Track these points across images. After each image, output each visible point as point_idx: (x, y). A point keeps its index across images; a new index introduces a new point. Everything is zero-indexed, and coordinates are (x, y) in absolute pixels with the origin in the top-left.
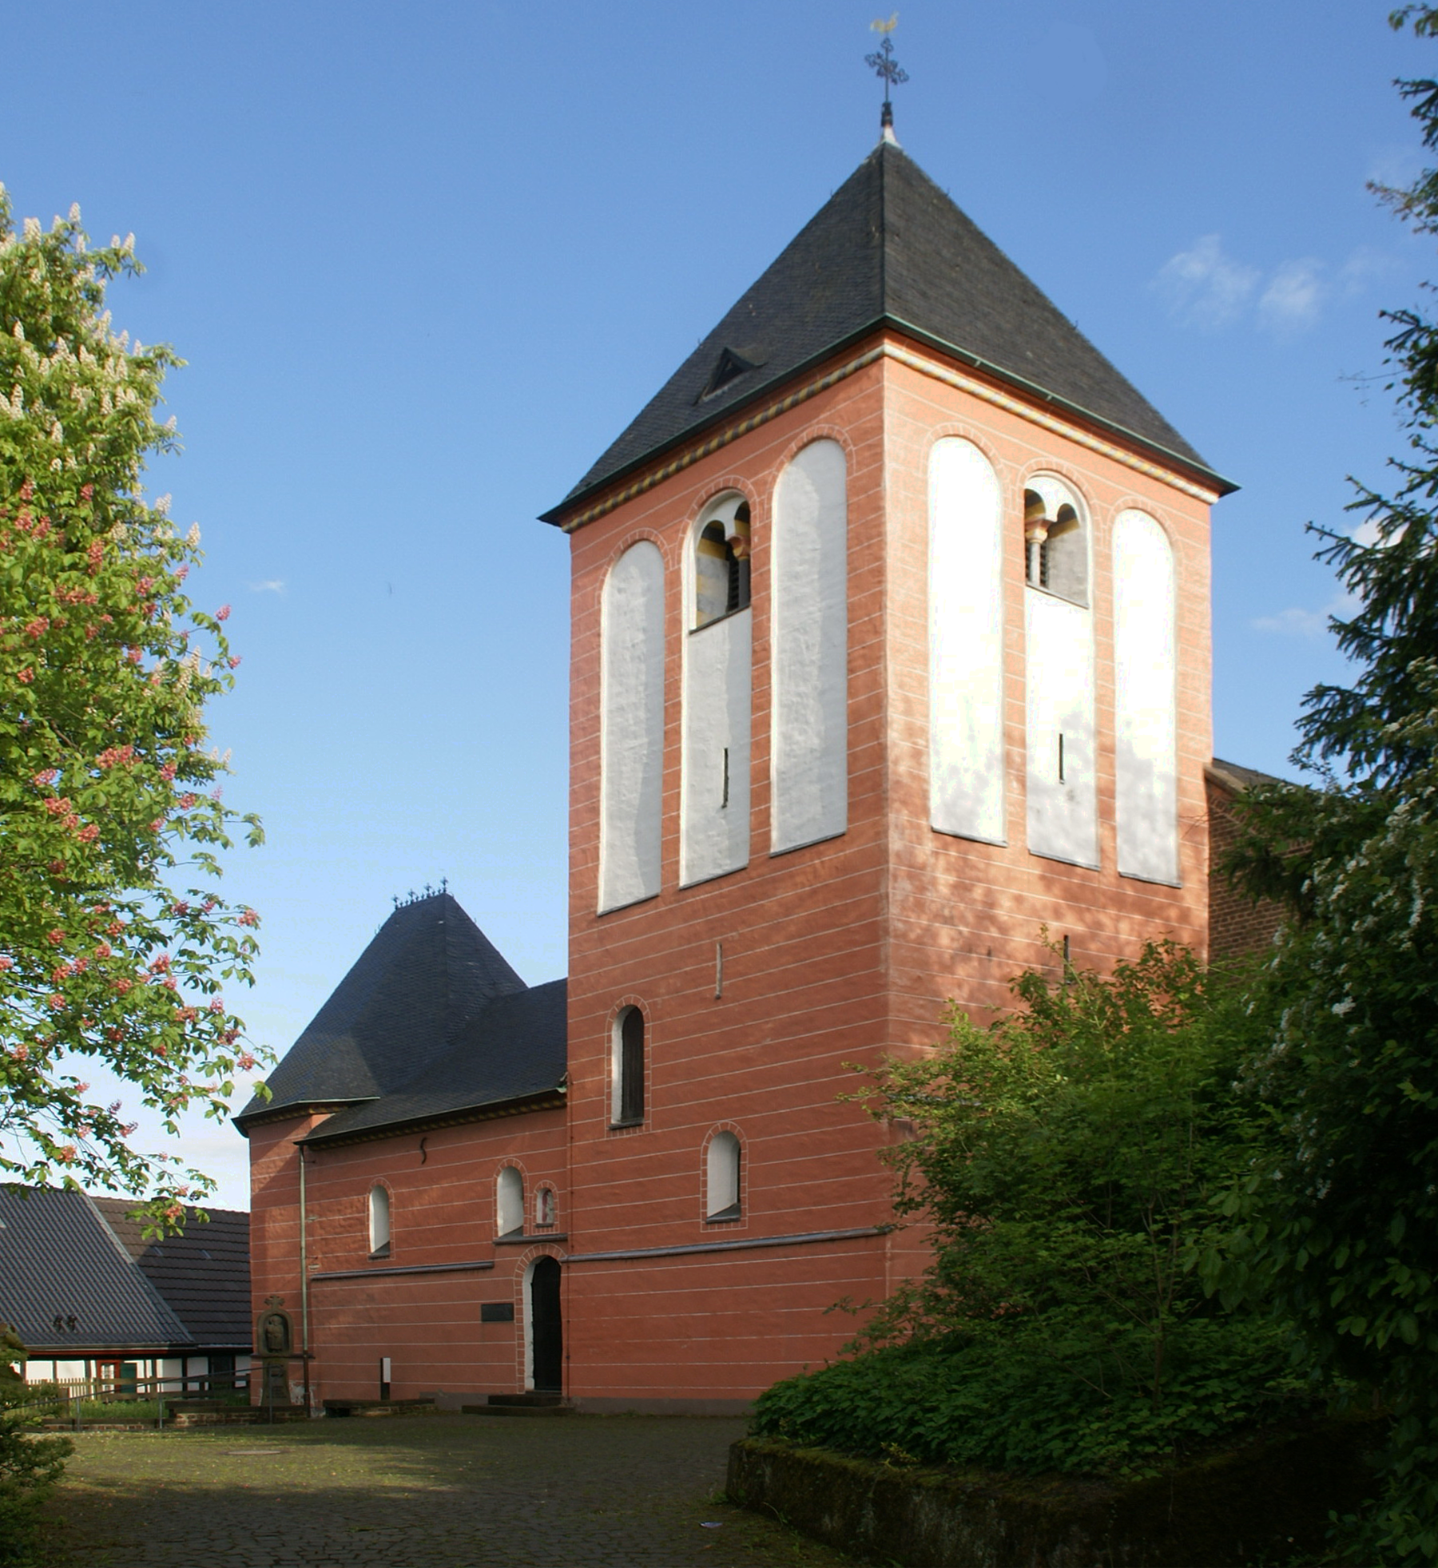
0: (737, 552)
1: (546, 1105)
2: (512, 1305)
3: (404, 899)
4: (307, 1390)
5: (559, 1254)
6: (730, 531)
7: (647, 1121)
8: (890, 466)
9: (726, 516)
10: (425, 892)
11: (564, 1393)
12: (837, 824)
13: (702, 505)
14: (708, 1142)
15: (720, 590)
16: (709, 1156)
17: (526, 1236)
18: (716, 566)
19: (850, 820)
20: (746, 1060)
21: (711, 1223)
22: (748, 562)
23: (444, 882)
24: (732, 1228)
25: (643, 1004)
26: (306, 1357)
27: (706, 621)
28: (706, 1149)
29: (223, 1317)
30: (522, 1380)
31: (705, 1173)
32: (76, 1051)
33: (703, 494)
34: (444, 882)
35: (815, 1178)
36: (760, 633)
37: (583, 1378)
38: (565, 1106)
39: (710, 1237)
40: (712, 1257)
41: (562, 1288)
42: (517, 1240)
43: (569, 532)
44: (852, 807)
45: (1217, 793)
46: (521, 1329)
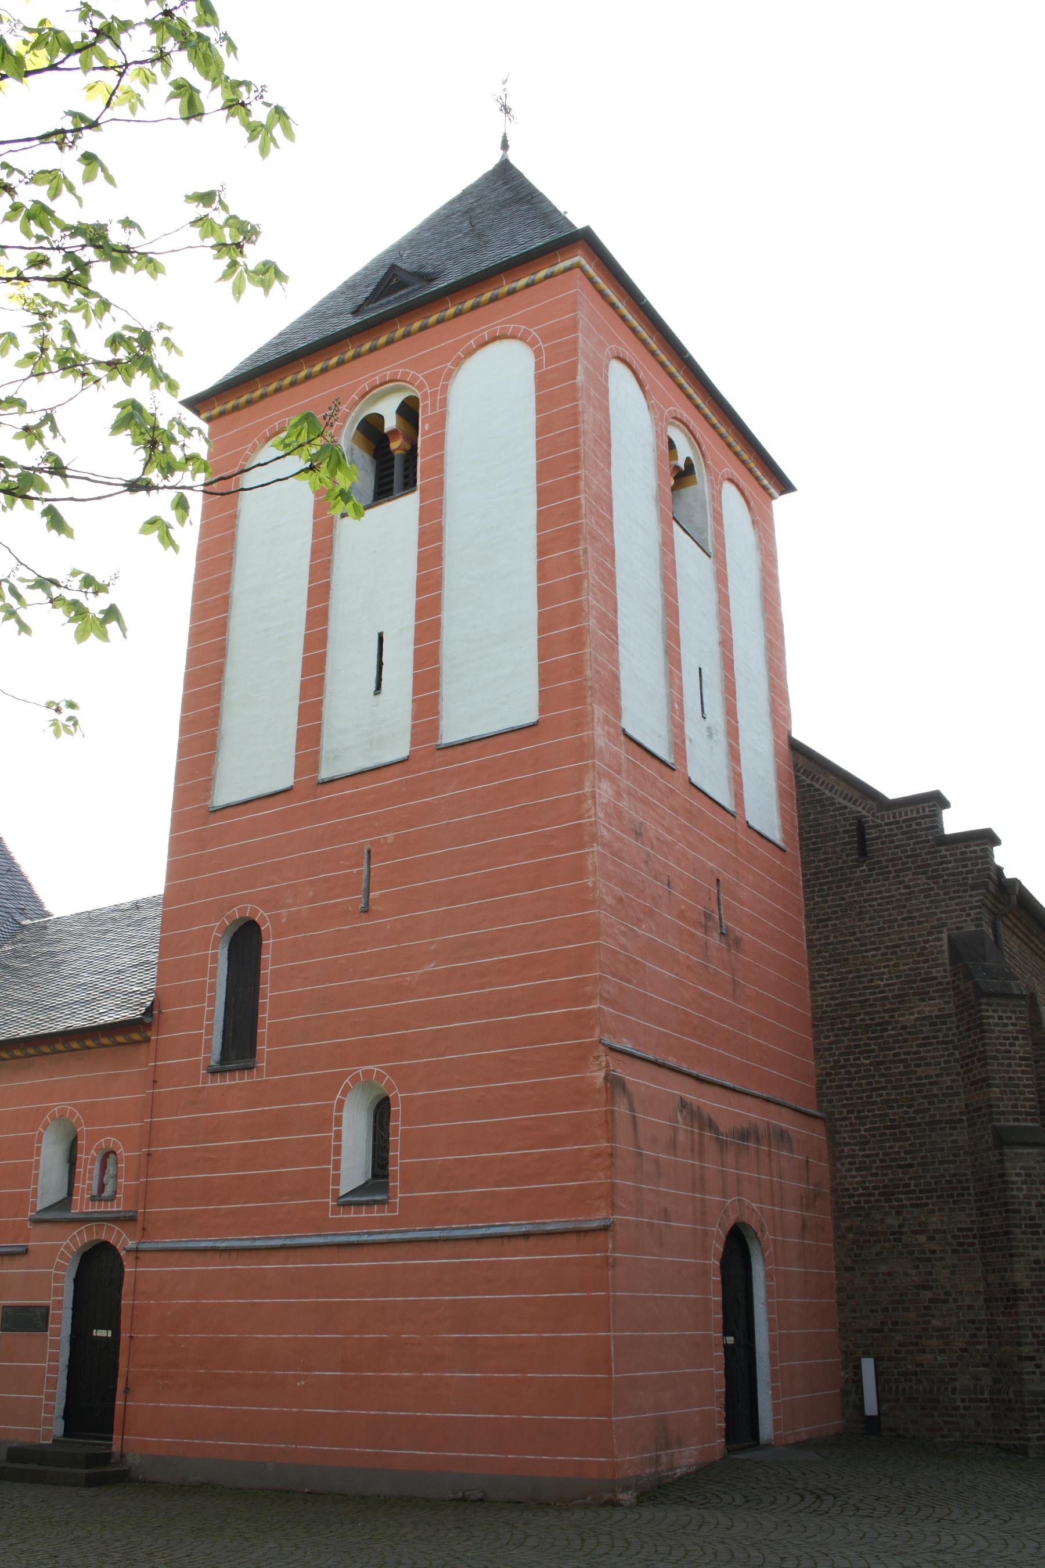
1: (120, 1039)
2: (47, 1308)
5: (123, 1240)
6: (391, 422)
9: (388, 410)
11: (116, 1448)
12: (531, 715)
14: (344, 1094)
16: (345, 1114)
19: (542, 709)
21: (345, 1203)
22: (411, 456)
25: (262, 916)
31: (338, 1136)
32: (45, 519)
37: (150, 1421)
41: (126, 1288)
43: (208, 420)
44: (544, 695)
45: (802, 761)
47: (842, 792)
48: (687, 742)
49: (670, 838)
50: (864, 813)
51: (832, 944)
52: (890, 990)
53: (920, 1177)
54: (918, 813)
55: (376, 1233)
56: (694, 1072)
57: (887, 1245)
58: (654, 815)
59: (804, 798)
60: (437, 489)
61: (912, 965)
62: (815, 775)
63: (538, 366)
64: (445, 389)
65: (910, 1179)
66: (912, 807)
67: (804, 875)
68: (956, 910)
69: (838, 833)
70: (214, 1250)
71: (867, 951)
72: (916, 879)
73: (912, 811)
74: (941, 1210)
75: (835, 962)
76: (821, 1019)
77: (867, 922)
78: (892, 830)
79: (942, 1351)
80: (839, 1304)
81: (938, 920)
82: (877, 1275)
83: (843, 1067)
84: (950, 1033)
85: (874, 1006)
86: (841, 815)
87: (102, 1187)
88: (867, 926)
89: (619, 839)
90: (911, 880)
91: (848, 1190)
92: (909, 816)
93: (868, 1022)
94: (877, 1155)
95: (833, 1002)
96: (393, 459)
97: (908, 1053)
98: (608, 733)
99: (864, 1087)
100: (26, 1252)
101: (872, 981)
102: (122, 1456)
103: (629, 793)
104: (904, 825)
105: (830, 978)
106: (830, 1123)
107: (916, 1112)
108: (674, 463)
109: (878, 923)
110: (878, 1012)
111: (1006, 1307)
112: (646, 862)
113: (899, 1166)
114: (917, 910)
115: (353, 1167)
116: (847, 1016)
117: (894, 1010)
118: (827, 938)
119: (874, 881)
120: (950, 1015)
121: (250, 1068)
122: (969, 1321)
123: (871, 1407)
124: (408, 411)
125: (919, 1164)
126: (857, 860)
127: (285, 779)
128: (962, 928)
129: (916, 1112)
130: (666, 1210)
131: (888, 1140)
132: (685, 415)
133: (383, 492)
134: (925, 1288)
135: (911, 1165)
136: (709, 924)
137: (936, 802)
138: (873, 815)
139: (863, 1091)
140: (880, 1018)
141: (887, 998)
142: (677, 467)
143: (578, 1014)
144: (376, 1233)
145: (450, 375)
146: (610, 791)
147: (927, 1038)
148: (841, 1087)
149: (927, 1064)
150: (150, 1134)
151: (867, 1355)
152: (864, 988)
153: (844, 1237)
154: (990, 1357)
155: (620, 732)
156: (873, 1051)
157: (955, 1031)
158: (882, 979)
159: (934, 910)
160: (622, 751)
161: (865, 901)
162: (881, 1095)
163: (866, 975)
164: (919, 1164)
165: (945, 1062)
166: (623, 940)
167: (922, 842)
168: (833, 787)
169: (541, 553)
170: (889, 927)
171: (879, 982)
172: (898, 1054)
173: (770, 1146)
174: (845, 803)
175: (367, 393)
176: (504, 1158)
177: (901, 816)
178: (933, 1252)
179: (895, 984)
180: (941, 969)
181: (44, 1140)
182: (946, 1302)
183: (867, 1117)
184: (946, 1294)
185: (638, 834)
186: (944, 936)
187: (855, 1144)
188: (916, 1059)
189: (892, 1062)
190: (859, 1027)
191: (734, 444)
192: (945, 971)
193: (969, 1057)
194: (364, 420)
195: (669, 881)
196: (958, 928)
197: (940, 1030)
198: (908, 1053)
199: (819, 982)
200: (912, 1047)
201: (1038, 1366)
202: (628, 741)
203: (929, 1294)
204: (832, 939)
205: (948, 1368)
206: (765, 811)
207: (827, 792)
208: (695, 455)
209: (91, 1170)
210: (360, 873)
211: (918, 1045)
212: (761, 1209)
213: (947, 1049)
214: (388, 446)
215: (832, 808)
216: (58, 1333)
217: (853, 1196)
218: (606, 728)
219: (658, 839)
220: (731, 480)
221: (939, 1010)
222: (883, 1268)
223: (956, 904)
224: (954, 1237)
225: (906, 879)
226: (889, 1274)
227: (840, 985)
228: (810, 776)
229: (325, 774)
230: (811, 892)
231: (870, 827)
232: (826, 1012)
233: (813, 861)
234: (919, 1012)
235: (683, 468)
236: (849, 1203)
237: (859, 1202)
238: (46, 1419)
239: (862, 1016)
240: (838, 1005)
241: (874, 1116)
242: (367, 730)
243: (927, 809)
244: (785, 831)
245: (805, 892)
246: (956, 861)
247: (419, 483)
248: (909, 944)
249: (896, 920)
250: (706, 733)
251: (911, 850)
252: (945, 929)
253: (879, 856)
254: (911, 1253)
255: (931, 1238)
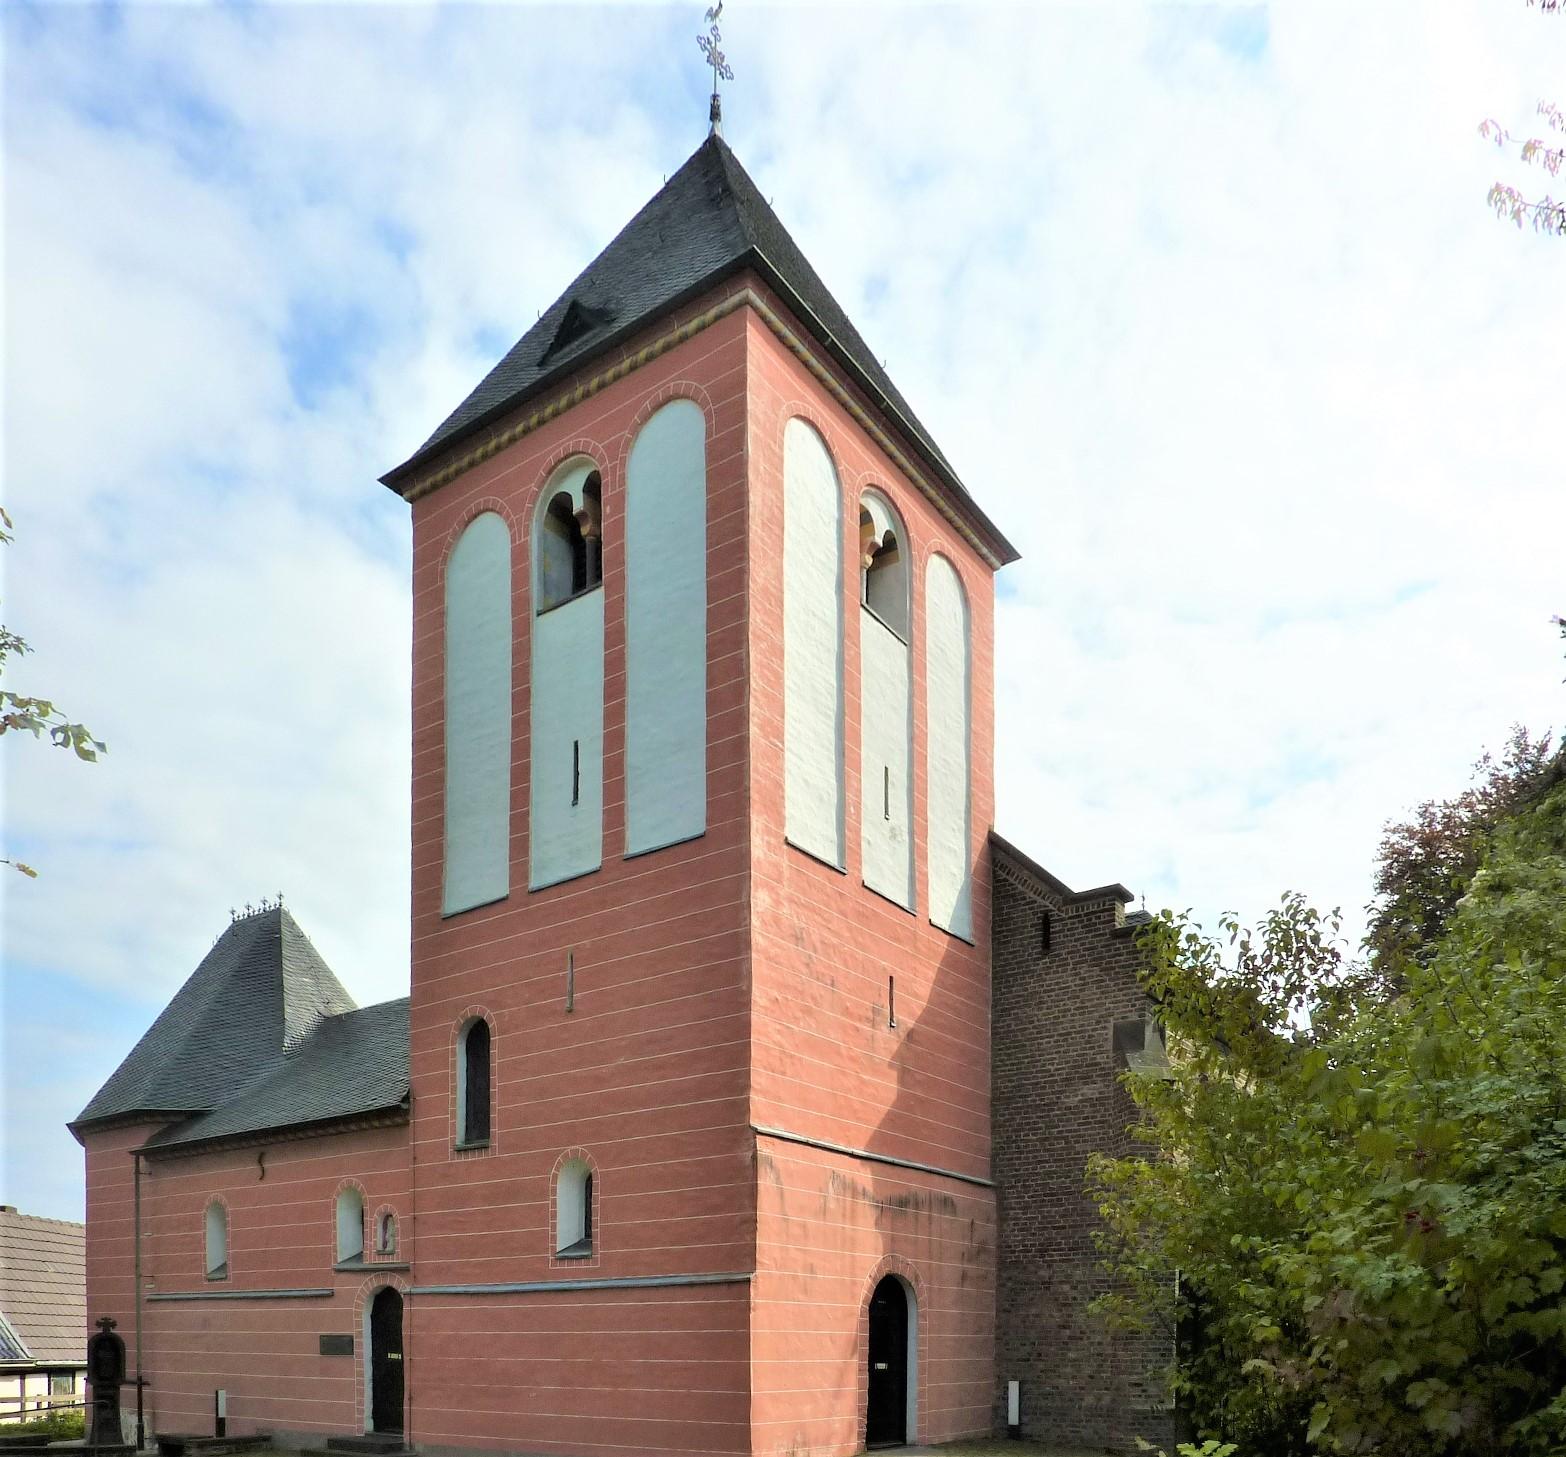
0: (585, 530)
1: (388, 1122)
3: (242, 912)
4: (140, 1419)
5: (402, 1286)
6: (578, 504)
7: (494, 1143)
8: (752, 429)
10: (262, 906)
11: (406, 1440)
12: (697, 826)
13: (549, 473)
14: (557, 1169)
15: (563, 572)
17: (366, 1264)
18: (560, 548)
19: (709, 821)
20: (599, 1080)
23: (280, 897)
24: (583, 1266)
25: (489, 1015)
26: (140, 1383)
27: (552, 602)
28: (555, 1177)
29: (62, 1331)
30: (361, 1421)
31: (554, 1203)
33: (552, 459)
34: (280, 897)
35: (672, 1214)
36: (614, 614)
38: (407, 1123)
39: (563, 1274)
40: (561, 1296)
41: (405, 1323)
42: (355, 1267)
43: (411, 500)
46: (361, 1365)
47: (1033, 886)
48: (864, 844)
49: (835, 941)
50: (1051, 907)
51: (1013, 1031)
52: (1059, 1075)
53: (1070, 1238)
54: (1099, 906)
55: (641, 1278)
56: (850, 1150)
57: (1039, 1293)
58: (819, 919)
59: (1000, 892)
60: (621, 578)
61: (1080, 1052)
62: (1010, 870)
63: (709, 434)
64: (623, 464)
65: (1062, 1239)
66: (1094, 901)
67: (994, 967)
68: (1123, 1001)
69: (1026, 927)
70: (466, 1294)
71: (1042, 1038)
72: (1090, 971)
73: (1093, 905)
74: (1084, 1265)
75: (1015, 1047)
76: (999, 1099)
77: (1045, 1011)
78: (1074, 923)
79: (1074, 1377)
80: (997, 1339)
81: (1106, 1010)
82: (1028, 1316)
83: (1014, 1142)
84: (1107, 1113)
85: (1044, 1088)
86: (1030, 909)
87: (385, 1244)
88: (1044, 1015)
89: (775, 945)
90: (1086, 972)
91: (1010, 1247)
92: (1091, 910)
93: (1038, 1102)
94: (1036, 1218)
95: (1009, 1084)
96: (585, 547)
97: (1070, 1131)
98: (768, 843)
99: (1031, 1160)
100: (331, 1295)
101: (1044, 1065)
102: (411, 1446)
103: (791, 901)
104: (1085, 918)
105: (1008, 1062)
106: (998, 1189)
107: (1073, 1182)
108: (869, 539)
109: (1053, 1013)
110: (1047, 1094)
111: (1125, 1344)
112: (807, 965)
113: (1054, 1228)
114: (1089, 1000)
115: (567, 1228)
116: (1020, 1097)
117: (1061, 1092)
118: (1009, 1026)
119: (1054, 972)
120: (1108, 1098)
121: (486, 1147)
122: (1098, 1355)
123: (1013, 1418)
124: (593, 488)
125: (1070, 1227)
126: (1040, 953)
127: (593, 861)
128: (1126, 1017)
129: (1073, 1182)
130: (812, 1265)
131: (1046, 1206)
132: (884, 478)
133: (581, 583)
134: (1064, 1327)
135: (1064, 1227)
136: (878, 1019)
137: (1119, 894)
138: (1059, 910)
139: (1029, 1164)
140: (1048, 1099)
141: (1056, 1081)
142: (874, 544)
143: (734, 1101)
144: (641, 1278)
145: (628, 445)
146: (768, 900)
147: (1087, 1118)
148: (1012, 1159)
149: (1084, 1141)
150: (414, 1202)
151: (1014, 1379)
152: (1037, 1072)
153: (1004, 1285)
154: (1111, 1383)
155: (782, 841)
156: (1040, 1128)
157: (1111, 1112)
158: (1053, 1064)
159: (1104, 1001)
160: (785, 859)
161: (1045, 992)
162: (1044, 1167)
163: (1039, 1061)
164: (1070, 1227)
165: (1100, 1139)
166: (778, 1037)
167: (1100, 935)
168: (1026, 881)
169: (710, 656)
170: (1064, 1016)
171: (1050, 1067)
172: (1061, 1132)
173: (930, 1210)
174: (1035, 897)
175: (554, 467)
176: (677, 1223)
177: (1083, 910)
178: (1075, 1299)
179: (1063, 1068)
180: (1105, 1055)
181: (338, 1205)
182: (1081, 1339)
183: (1030, 1186)
184: (1081, 1332)
185: (798, 939)
186: (1111, 1026)
187: (1019, 1209)
188: (1075, 1137)
189: (1056, 1138)
190: (1028, 1107)
191: (946, 508)
192: (1108, 1057)
193: (1119, 1135)
194: (552, 500)
195: (833, 981)
196: (1123, 1018)
197: (1098, 1111)
198: (1070, 1131)
199: (998, 1066)
200: (1073, 1125)
201: (1144, 1391)
202: (791, 850)
203: (1068, 1332)
204: (1013, 1027)
205: (1078, 1391)
206: (948, 900)
207: (1020, 886)
208: (896, 528)
209: (376, 1231)
210: (564, 977)
211: (1079, 1125)
212: (916, 1263)
213: (1103, 1128)
214: (580, 532)
215: (1023, 902)
216: (360, 1356)
217: (1014, 1252)
218: (766, 838)
219: (823, 942)
220: (940, 554)
221: (1100, 1093)
222: (1034, 1311)
223: (1124, 995)
224: (1093, 1287)
225: (1082, 971)
226: (1037, 1316)
227: (1017, 1069)
228: (1003, 873)
229: (534, 884)
230: (999, 983)
231: (1056, 921)
232: (1004, 1093)
233: (1002, 954)
234: (1082, 1095)
235: (881, 545)
236: (1011, 1257)
237: (1019, 1257)
238: (358, 1419)
239: (1034, 1097)
240: (1014, 1087)
241: (1037, 1185)
242: (568, 845)
243: (1107, 903)
244: (976, 926)
245: (993, 983)
246: (1128, 953)
247: (603, 577)
248: (1079, 1032)
249: (1069, 1010)
250: (888, 834)
251: (1090, 943)
252: (1111, 1019)
253: (1060, 949)
254: (1056, 1300)
255: (1075, 1288)
